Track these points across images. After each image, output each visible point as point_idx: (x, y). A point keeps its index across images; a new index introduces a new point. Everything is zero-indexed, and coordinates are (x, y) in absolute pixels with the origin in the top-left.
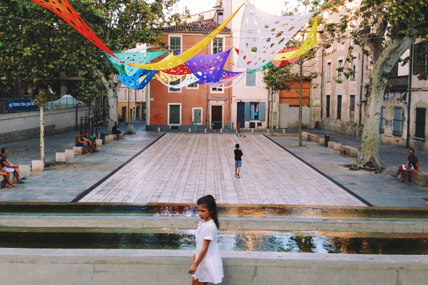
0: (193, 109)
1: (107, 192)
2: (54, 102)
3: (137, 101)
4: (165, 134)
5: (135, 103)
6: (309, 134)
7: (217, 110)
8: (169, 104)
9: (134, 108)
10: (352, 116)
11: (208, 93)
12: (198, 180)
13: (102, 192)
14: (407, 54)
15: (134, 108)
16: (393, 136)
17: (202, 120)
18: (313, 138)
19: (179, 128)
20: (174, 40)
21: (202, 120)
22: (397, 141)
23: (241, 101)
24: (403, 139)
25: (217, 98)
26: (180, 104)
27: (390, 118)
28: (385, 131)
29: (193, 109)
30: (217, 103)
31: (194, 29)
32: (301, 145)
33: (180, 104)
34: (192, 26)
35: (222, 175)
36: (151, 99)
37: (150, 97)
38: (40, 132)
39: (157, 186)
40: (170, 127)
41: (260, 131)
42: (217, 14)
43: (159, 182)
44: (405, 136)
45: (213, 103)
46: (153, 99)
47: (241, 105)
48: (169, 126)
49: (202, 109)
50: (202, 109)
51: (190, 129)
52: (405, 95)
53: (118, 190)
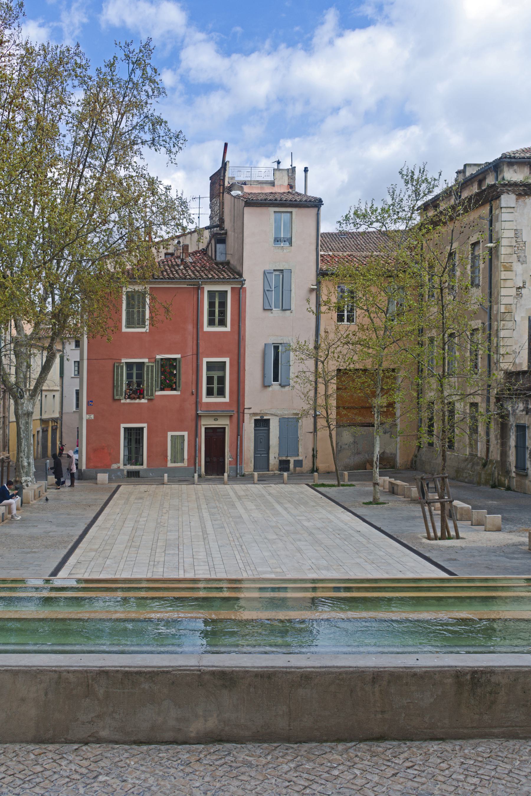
3: (45, 417)
4: (119, 487)
5: (39, 422)
6: (392, 480)
7: (215, 438)
8: (123, 426)
9: (38, 432)
10: (473, 445)
11: (197, 403)
14: (225, 508)
15: (38, 432)
18: (399, 490)
19: (141, 474)
20: (133, 297)
23: (262, 417)
25: (215, 412)
30: (217, 423)
31: (172, 276)
32: (375, 502)
33: (145, 425)
34: (167, 267)
36: (88, 416)
37: (87, 413)
40: (125, 473)
41: (301, 475)
42: (213, 242)
45: (207, 423)
46: (92, 416)
48: (123, 470)
50: (186, 434)
51: (166, 475)
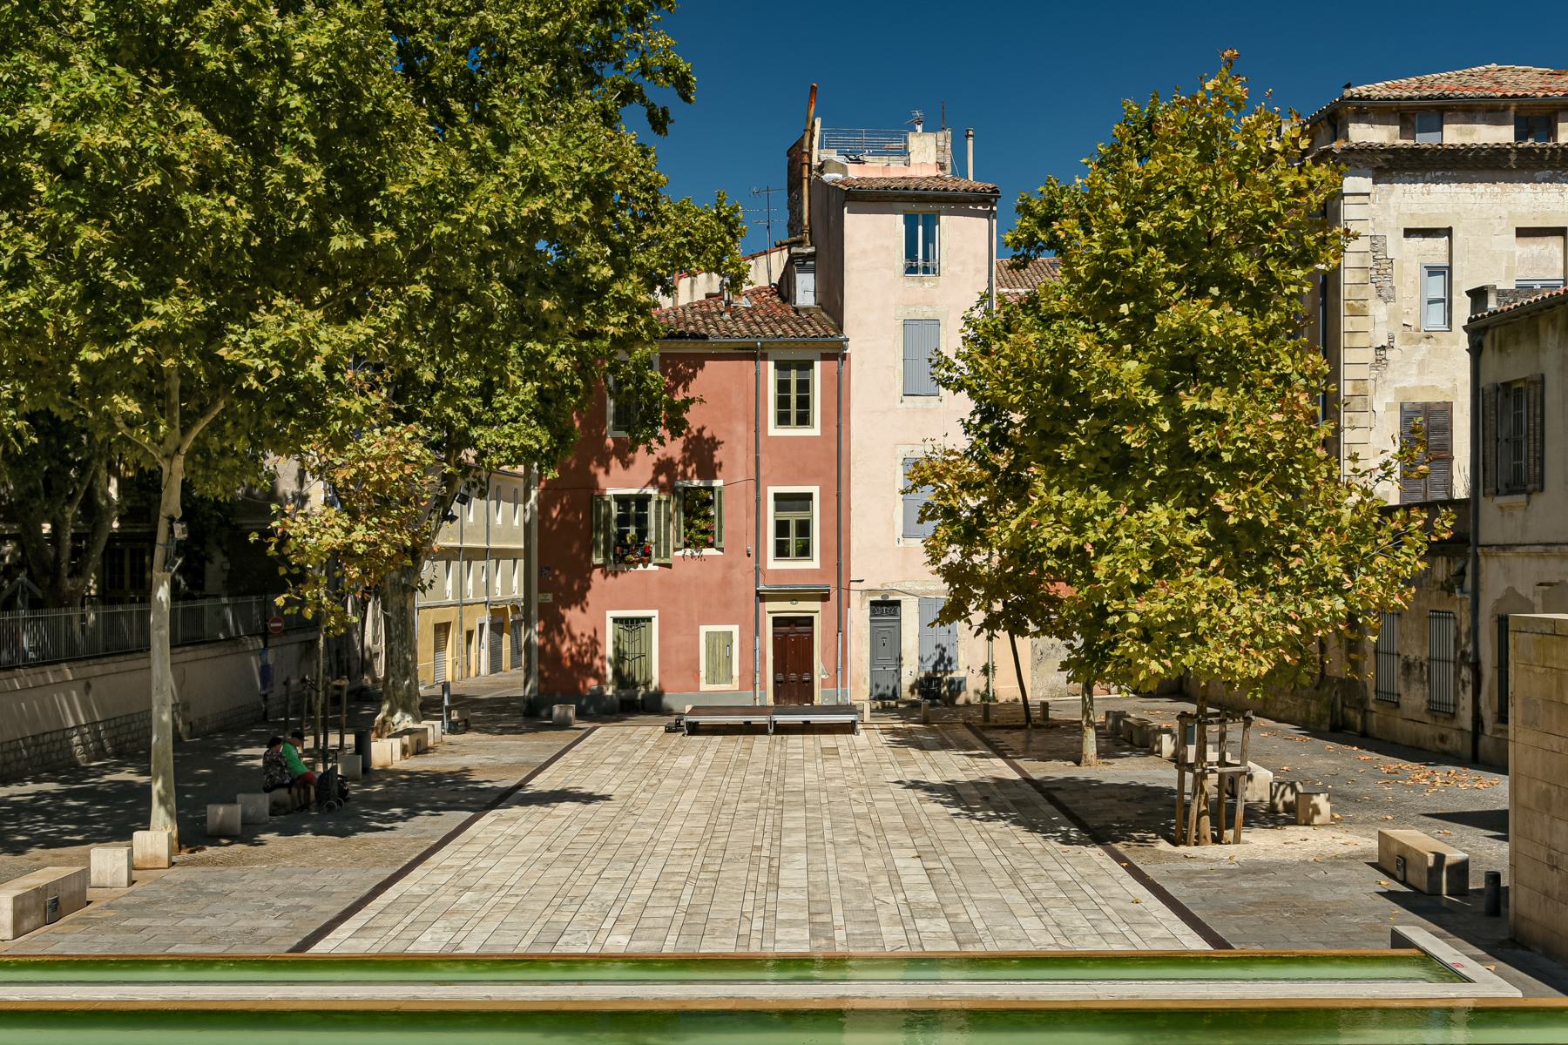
0: (703, 629)
1: (383, 932)
2: (457, 544)
4: (595, 729)
12: (688, 890)
13: (365, 933)
16: (1428, 719)
17: (736, 672)
21: (736, 672)
22: (1443, 739)
24: (1461, 730)
26: (654, 613)
27: (1417, 653)
28: (1403, 701)
29: (703, 629)
35: (774, 872)
36: (541, 597)
38: (1446, 428)
39: (549, 911)
43: (558, 901)
44: (1466, 720)
47: (898, 603)
49: (735, 629)
50: (735, 629)
52: (1462, 572)
53: (578, 901)
